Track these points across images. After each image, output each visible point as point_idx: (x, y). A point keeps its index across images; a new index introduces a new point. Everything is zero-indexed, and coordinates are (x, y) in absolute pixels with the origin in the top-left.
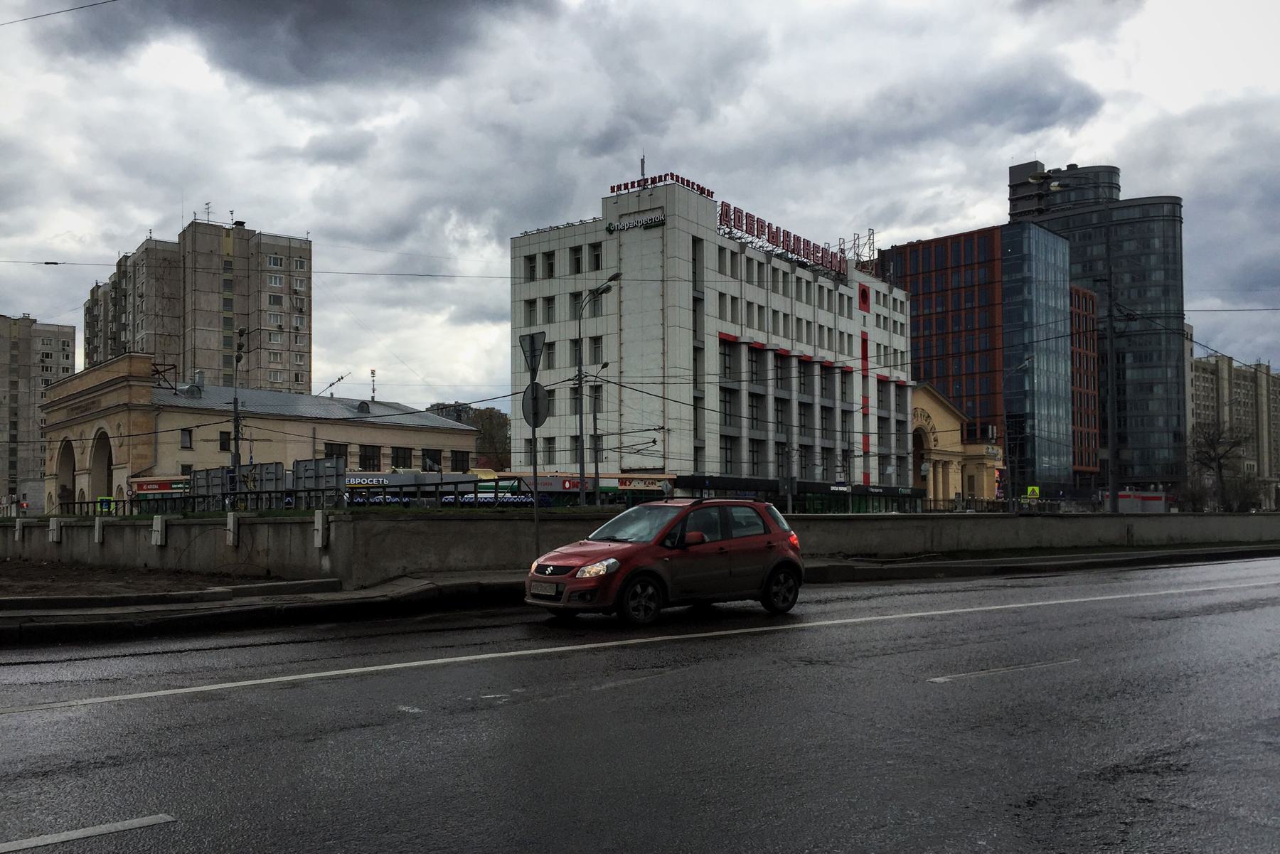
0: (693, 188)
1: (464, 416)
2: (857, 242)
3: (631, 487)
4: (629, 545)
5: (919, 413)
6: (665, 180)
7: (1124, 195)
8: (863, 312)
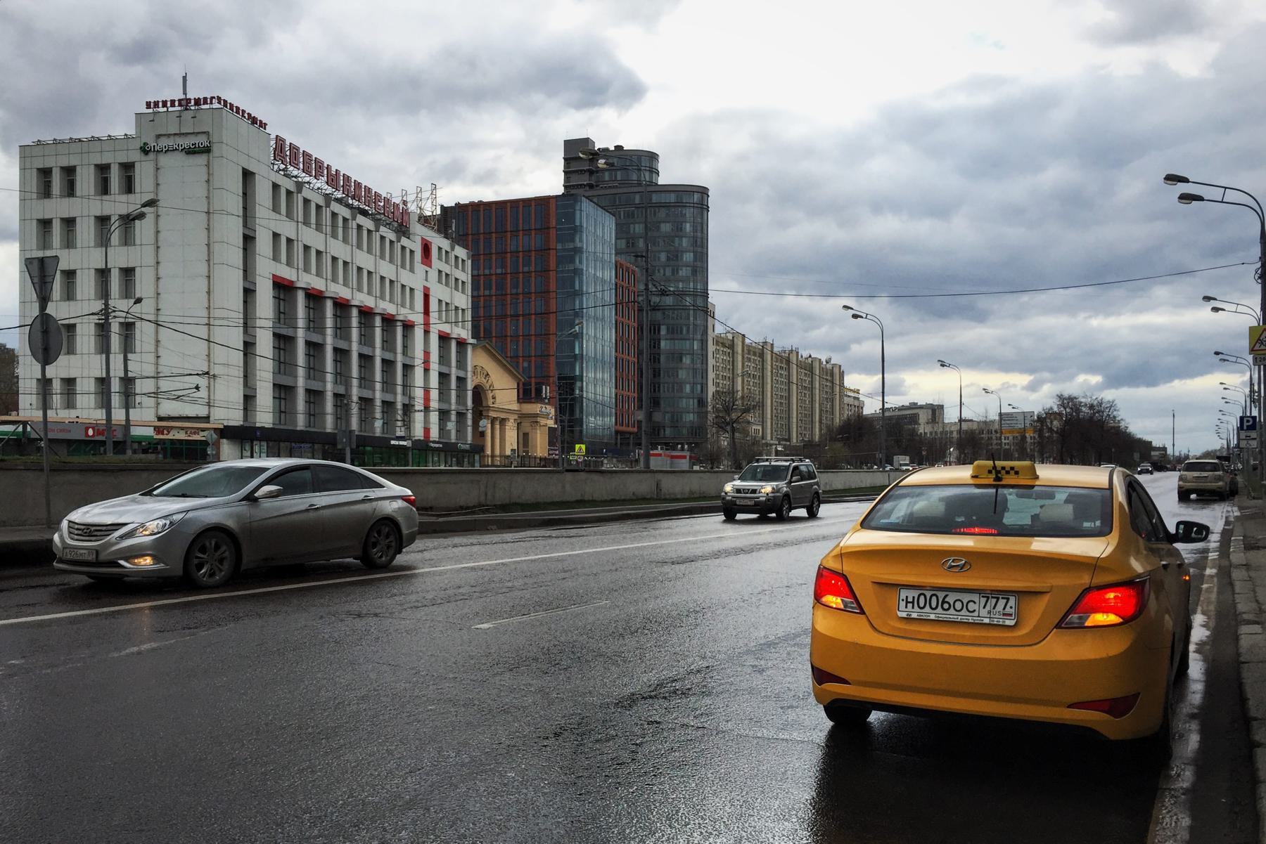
0: (243, 116)
6: (211, 103)
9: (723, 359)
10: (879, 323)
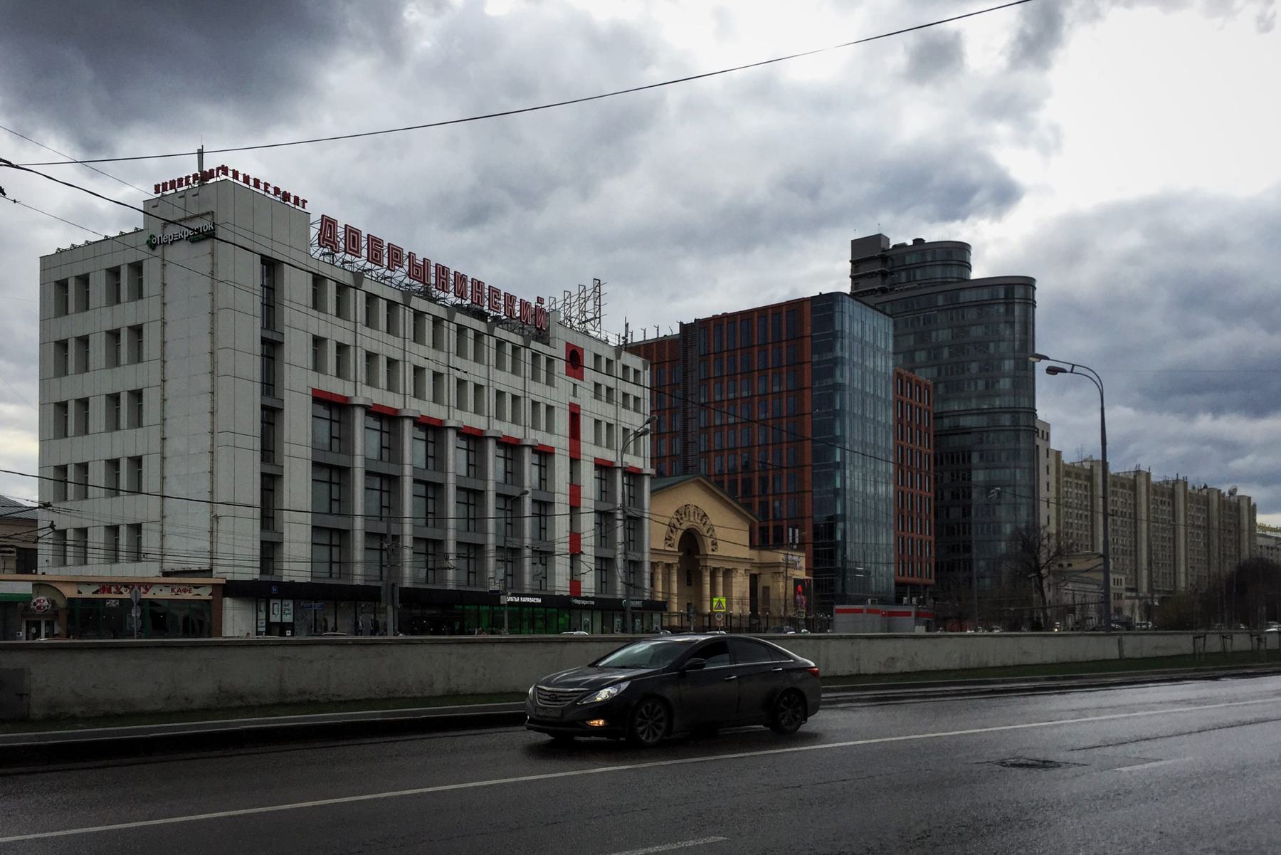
0: (266, 190)
2: (583, 295)
3: (149, 595)
4: (613, 690)
5: (692, 512)
6: (218, 176)
7: (976, 273)
8: (572, 379)
9: (1077, 494)
10: (1096, 379)
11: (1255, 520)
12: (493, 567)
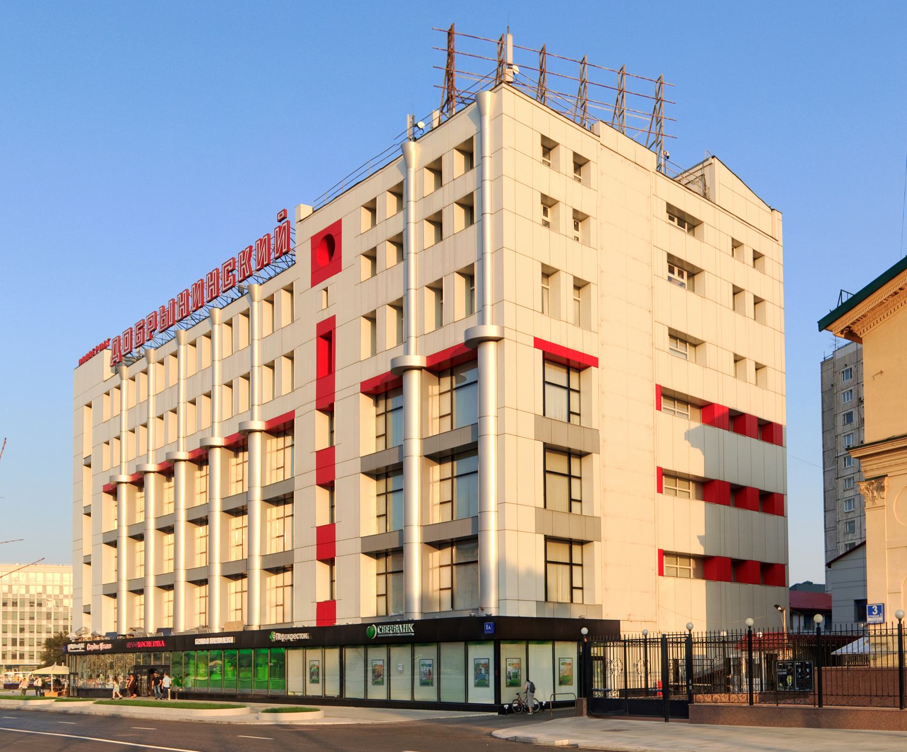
1: (548, 164)
11: (218, 633)
12: (612, 644)
